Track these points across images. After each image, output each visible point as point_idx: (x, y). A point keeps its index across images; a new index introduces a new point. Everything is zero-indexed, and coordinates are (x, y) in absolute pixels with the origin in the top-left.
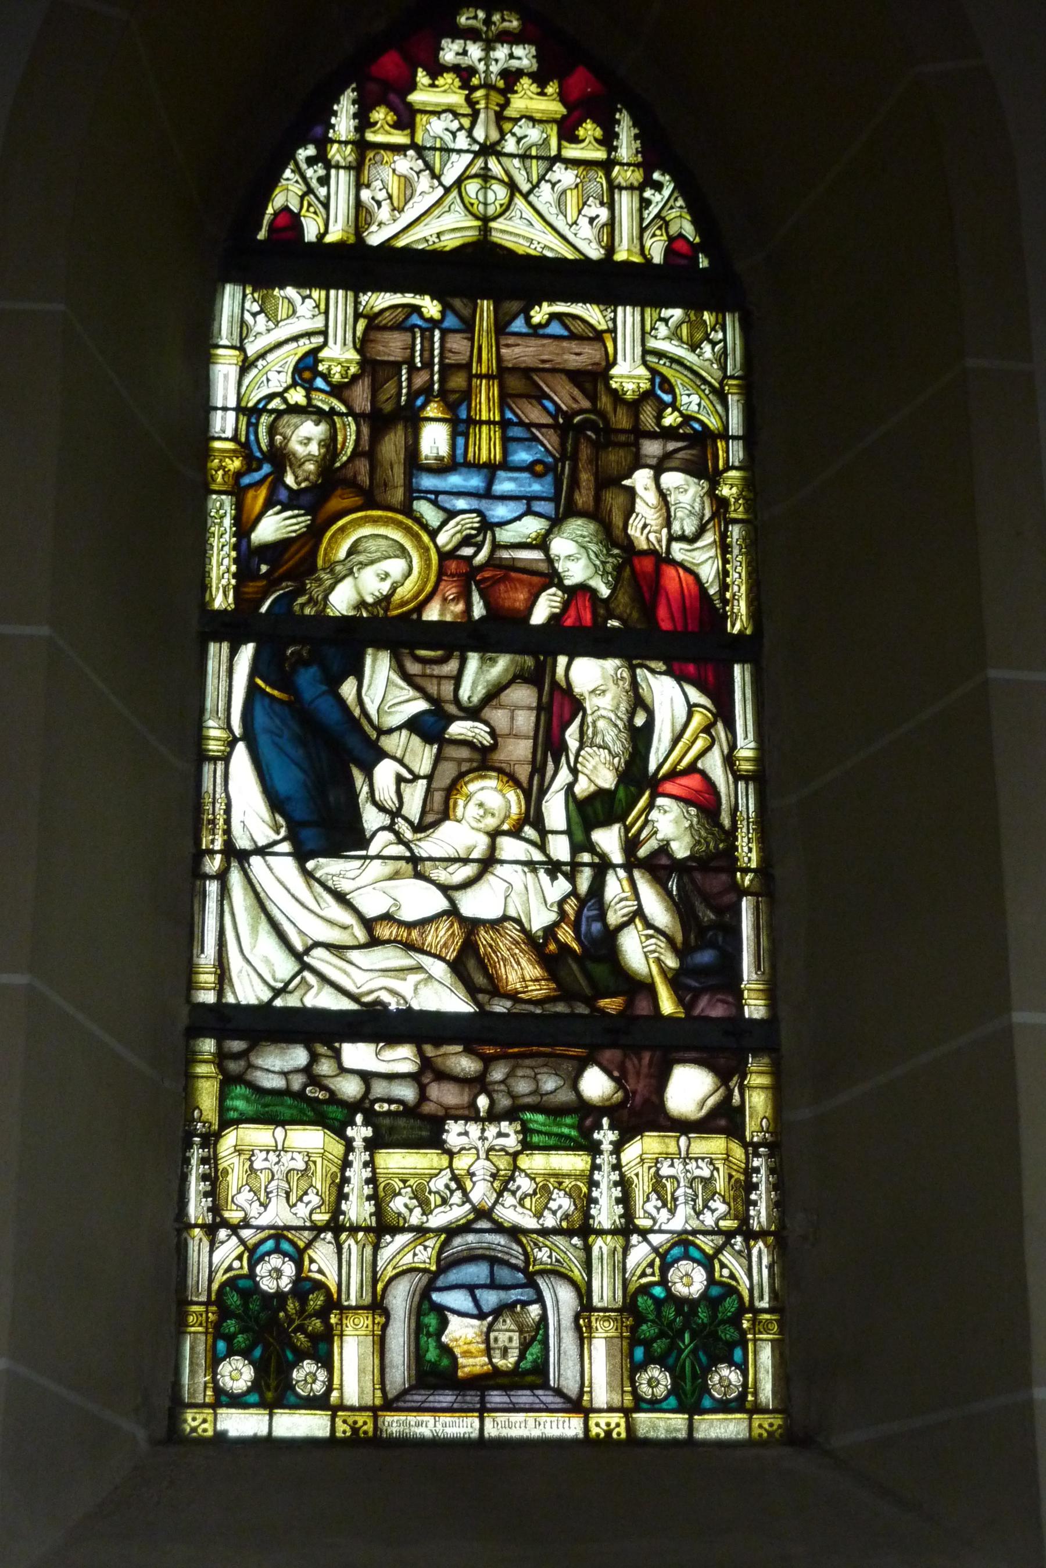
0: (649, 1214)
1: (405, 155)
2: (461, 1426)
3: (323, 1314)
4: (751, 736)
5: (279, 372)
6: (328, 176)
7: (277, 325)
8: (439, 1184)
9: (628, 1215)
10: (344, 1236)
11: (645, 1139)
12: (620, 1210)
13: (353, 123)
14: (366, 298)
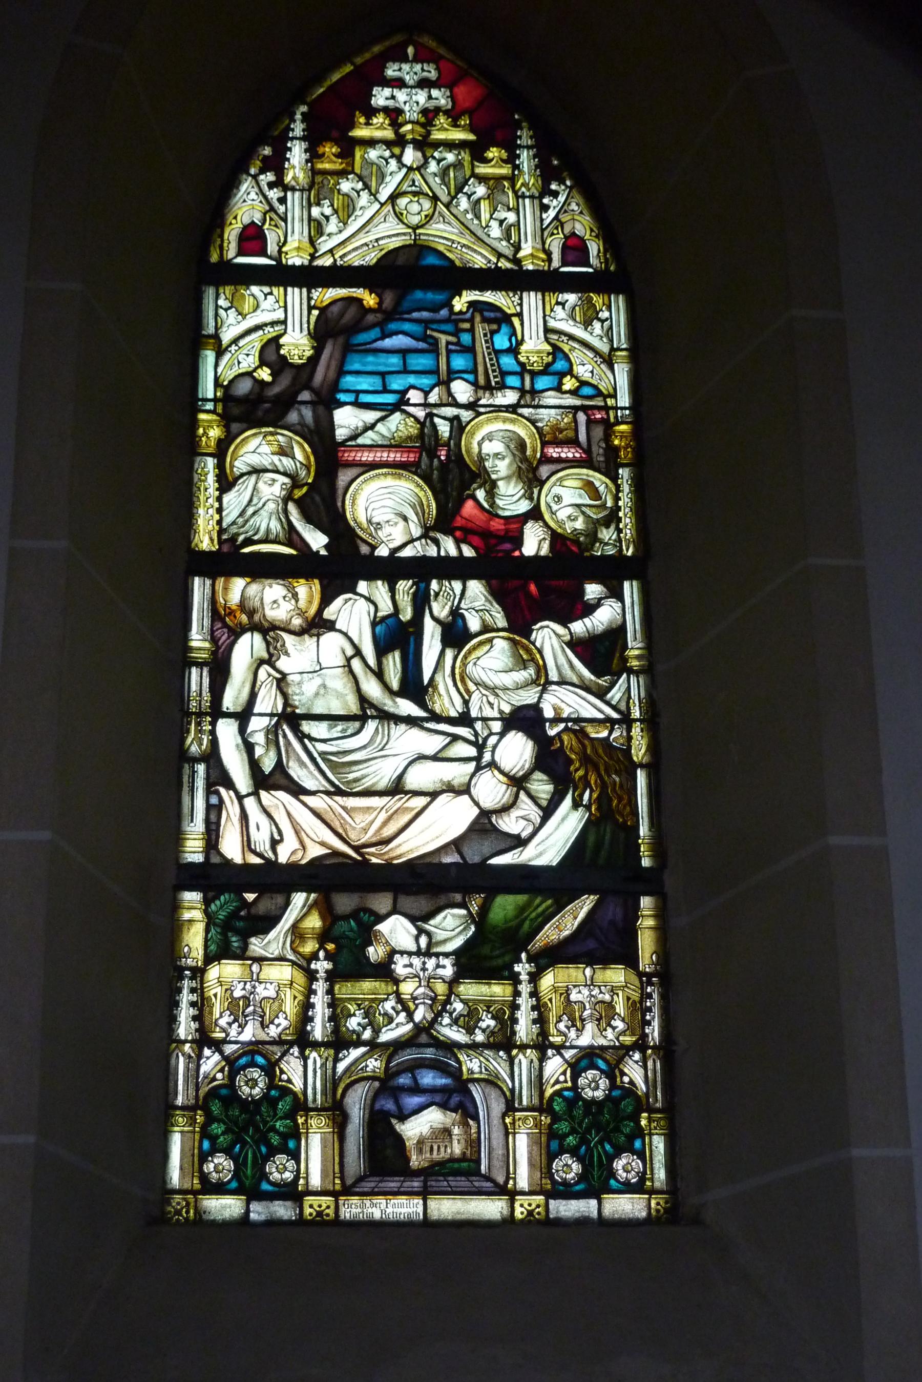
0: (561, 1032)
1: (348, 179)
2: (405, 1208)
3: (291, 1115)
4: (638, 635)
5: (248, 355)
6: (285, 196)
7: (244, 318)
8: (389, 1006)
9: (544, 1033)
10: (515, 1052)
11: (556, 970)
12: (535, 1029)
13: (305, 156)
14: (317, 294)
